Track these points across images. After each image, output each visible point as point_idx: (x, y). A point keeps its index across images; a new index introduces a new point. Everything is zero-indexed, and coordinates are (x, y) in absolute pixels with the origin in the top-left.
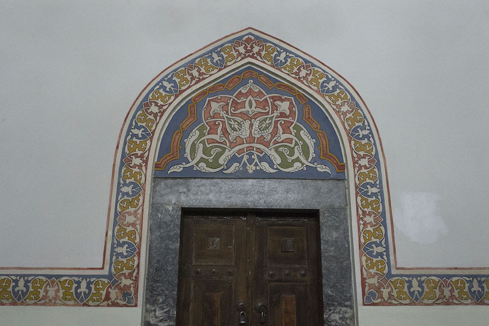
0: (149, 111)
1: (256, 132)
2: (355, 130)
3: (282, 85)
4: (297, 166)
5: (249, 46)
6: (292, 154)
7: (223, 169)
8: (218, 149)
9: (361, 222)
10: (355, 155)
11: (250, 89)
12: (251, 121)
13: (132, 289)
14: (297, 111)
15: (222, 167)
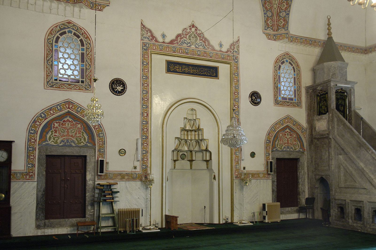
4: (297, 150)
6: (81, 140)
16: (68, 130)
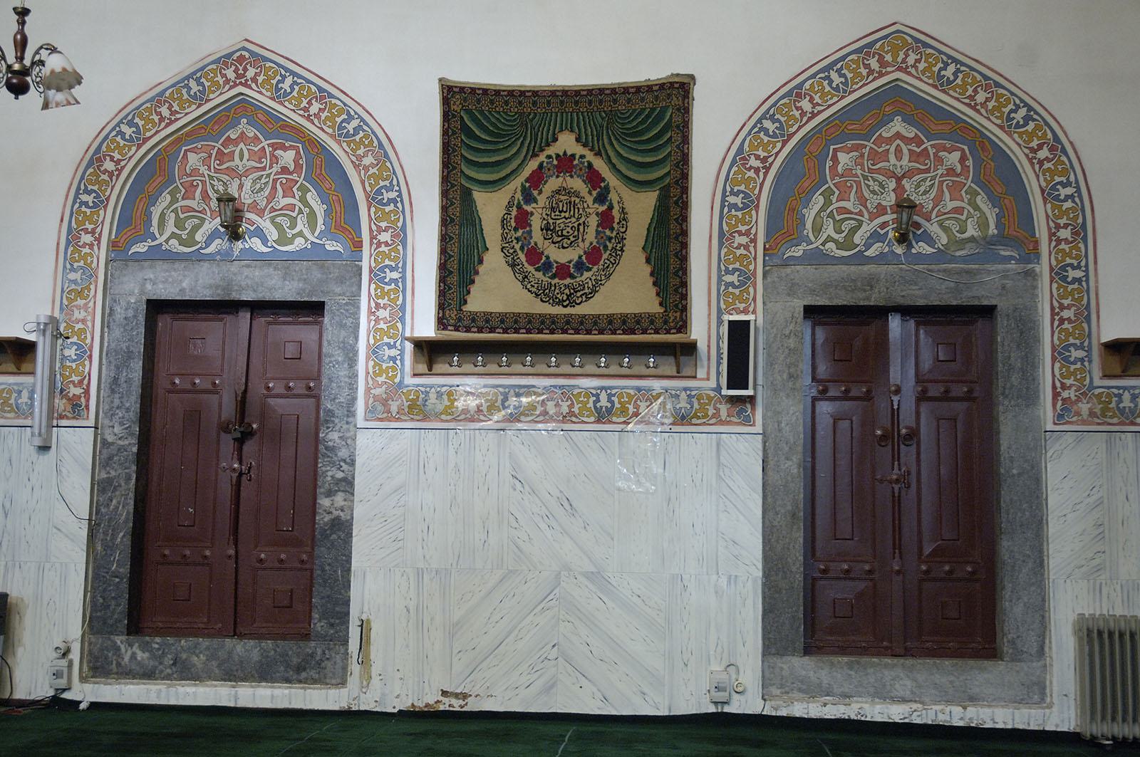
0: (102, 169)
1: (247, 196)
2: (379, 192)
3: (287, 126)
4: (299, 243)
5: (241, 68)
6: (293, 226)
7: (201, 248)
8: (195, 220)
9: (373, 318)
10: (374, 227)
11: (243, 133)
12: (240, 180)
13: (83, 400)
14: (304, 165)
15: (200, 245)
16: (899, 180)
